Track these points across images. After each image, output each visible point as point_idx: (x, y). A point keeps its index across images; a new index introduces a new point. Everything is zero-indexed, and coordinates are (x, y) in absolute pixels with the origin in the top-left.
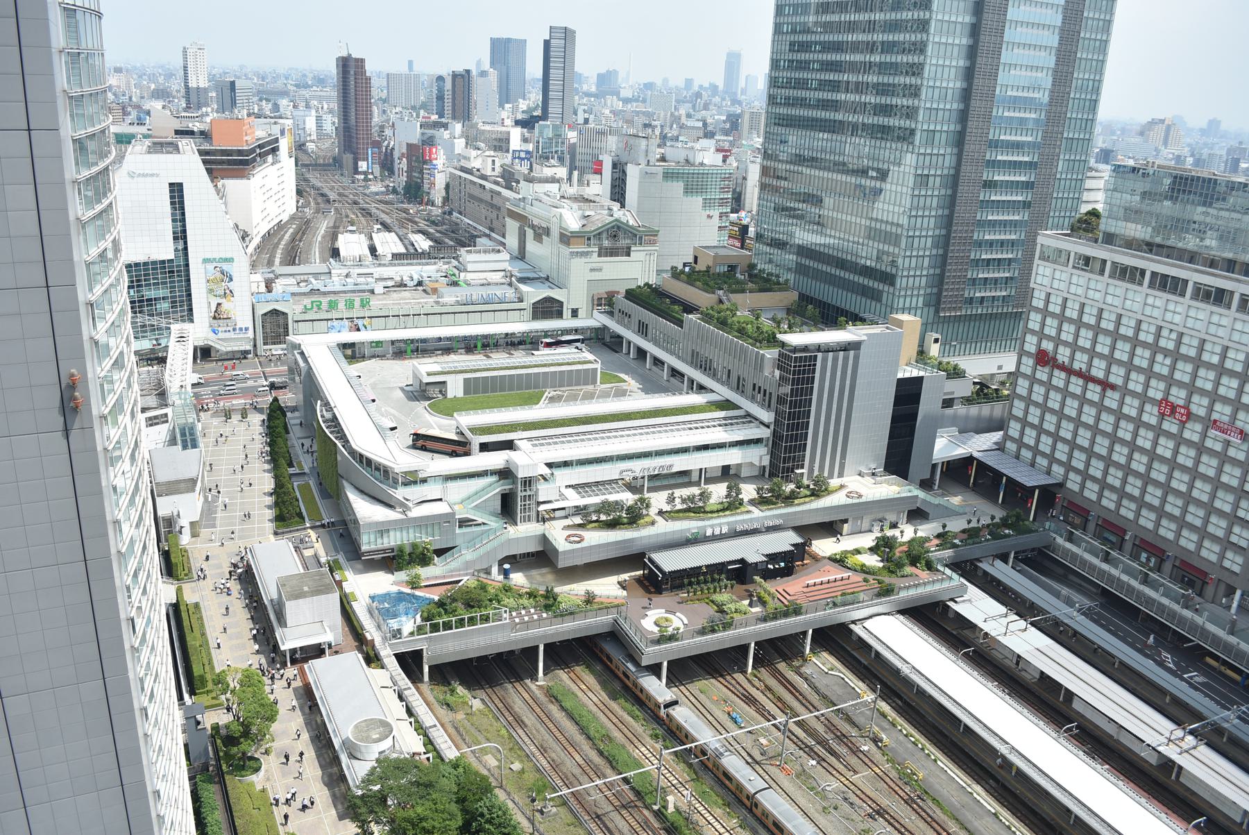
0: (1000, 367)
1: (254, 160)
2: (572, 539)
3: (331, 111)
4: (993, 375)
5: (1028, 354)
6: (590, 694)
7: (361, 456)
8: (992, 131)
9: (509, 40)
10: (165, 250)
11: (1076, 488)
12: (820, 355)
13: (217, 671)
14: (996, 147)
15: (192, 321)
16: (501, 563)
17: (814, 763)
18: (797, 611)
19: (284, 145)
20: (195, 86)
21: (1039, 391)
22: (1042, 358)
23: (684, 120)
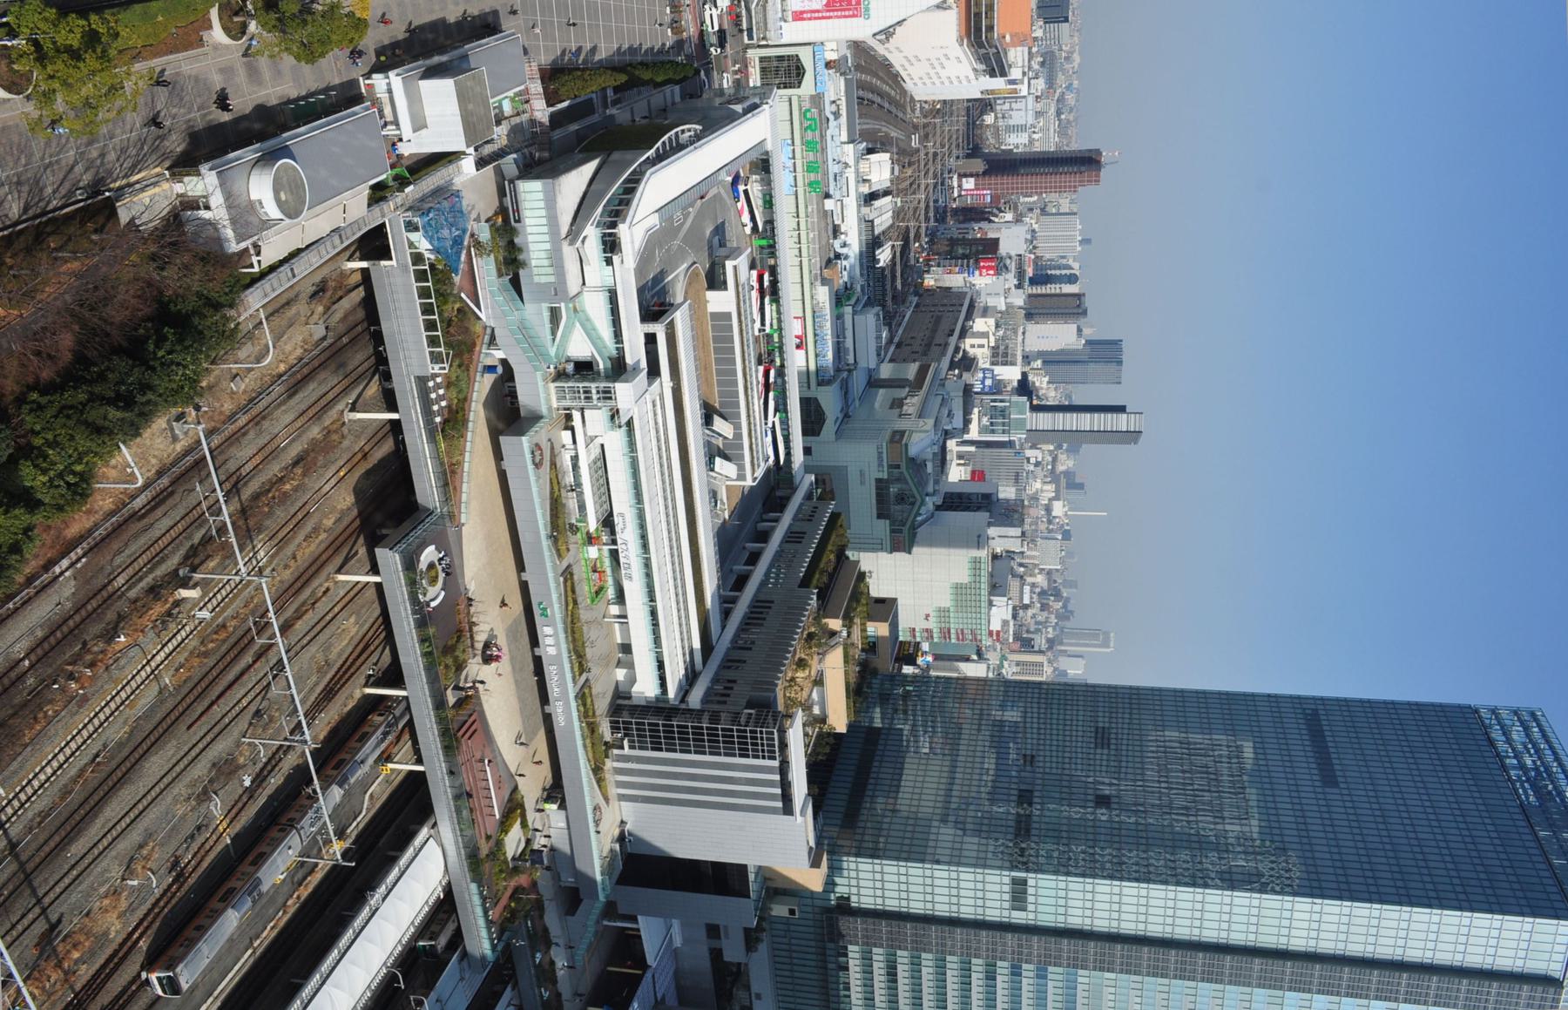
0: (759, 996)
2: (537, 453)
3: (1031, 141)
6: (333, 481)
8: (1060, 970)
9: (1120, 363)
12: (776, 763)
14: (1013, 974)
16: (504, 362)
17: (247, 783)
18: (1121, 409)
19: (998, 83)
23: (1029, 580)
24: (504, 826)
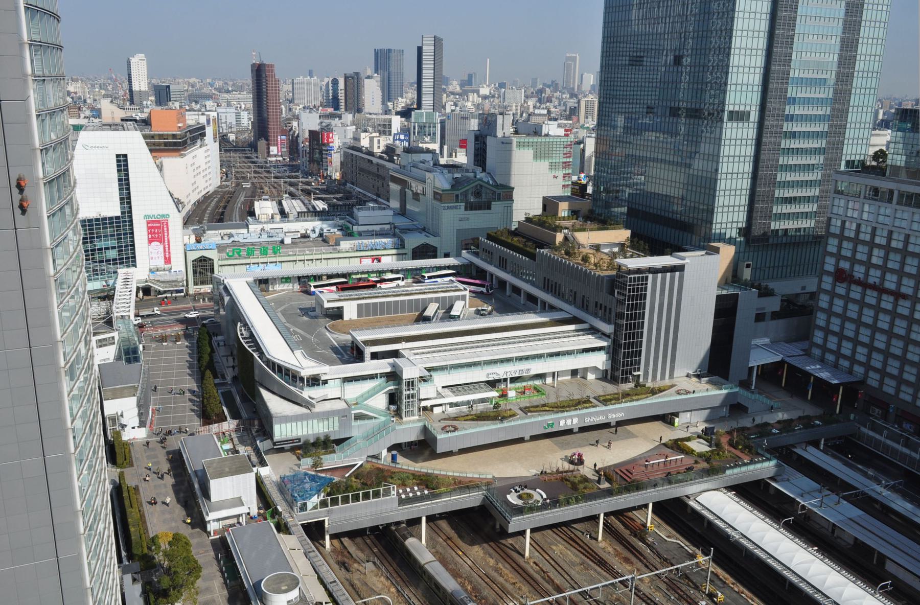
0: (804, 288)
1: (185, 143)
2: (448, 429)
3: (246, 109)
4: (797, 295)
5: (828, 273)
7: (274, 363)
9: (389, 51)
10: (114, 210)
11: (875, 384)
12: (650, 276)
13: (151, 536)
15: (135, 266)
18: (420, 50)
19: (209, 131)
20: (137, 89)
21: (838, 305)
22: (840, 276)
24: (689, 452)
